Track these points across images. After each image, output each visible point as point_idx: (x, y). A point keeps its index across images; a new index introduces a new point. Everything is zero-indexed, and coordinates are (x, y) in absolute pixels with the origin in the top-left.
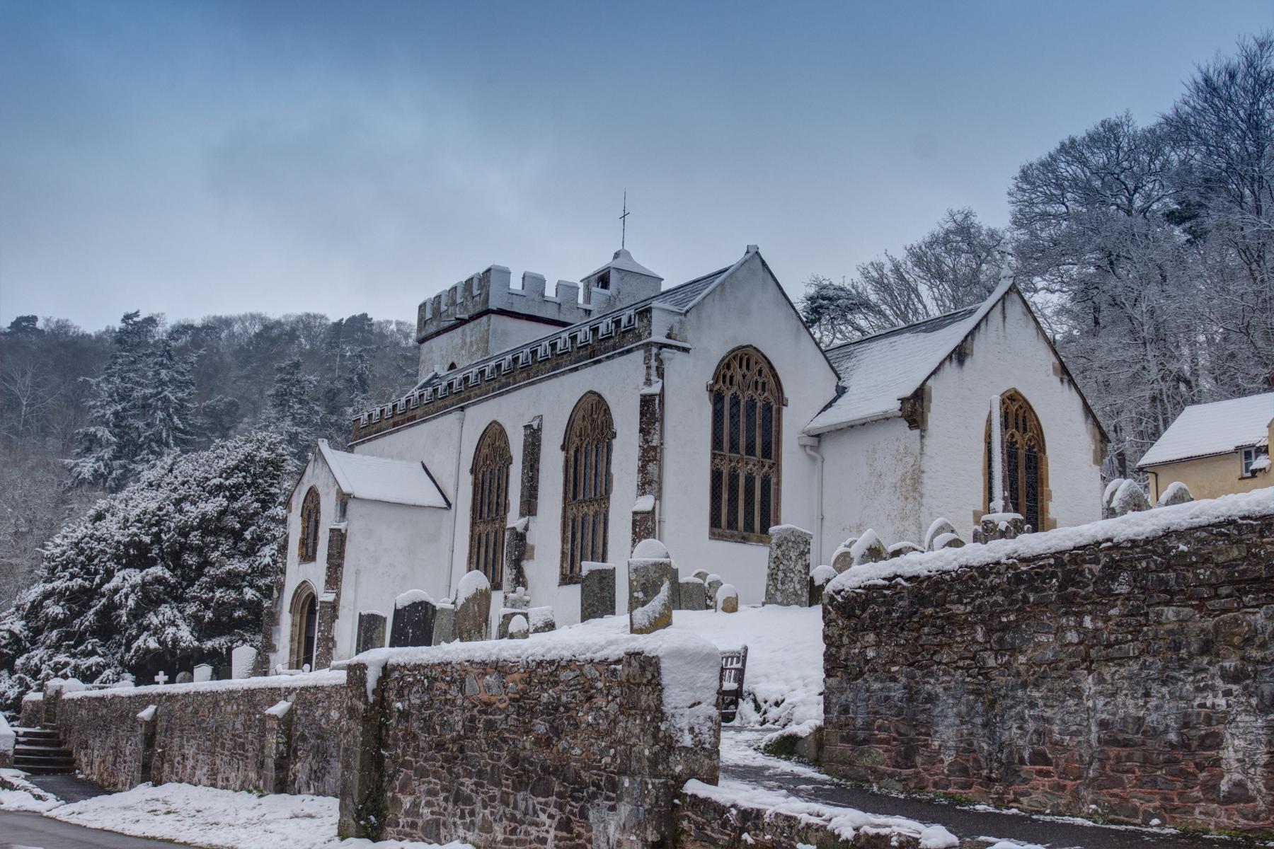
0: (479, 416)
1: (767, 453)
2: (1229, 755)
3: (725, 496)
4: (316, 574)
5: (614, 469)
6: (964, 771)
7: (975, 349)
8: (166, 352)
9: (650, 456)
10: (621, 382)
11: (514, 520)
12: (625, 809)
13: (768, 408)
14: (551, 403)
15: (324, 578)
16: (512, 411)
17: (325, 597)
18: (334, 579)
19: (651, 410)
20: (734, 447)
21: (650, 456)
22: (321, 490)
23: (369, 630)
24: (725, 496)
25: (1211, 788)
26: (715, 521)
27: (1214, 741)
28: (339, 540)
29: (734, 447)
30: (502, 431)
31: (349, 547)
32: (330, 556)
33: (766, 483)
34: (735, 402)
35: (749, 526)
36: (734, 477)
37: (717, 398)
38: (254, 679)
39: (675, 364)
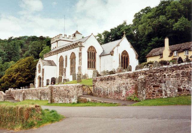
0: (60, 55)
1: (94, 59)
2: (123, 93)
3: (89, 64)
4: (41, 74)
5: (76, 62)
6: (104, 95)
7: (46, 81)
8: (14, 40)
9: (80, 60)
10: (76, 51)
11: (64, 67)
12: (74, 99)
13: (94, 53)
14: (68, 53)
15: (42, 75)
16: (63, 54)
17: (41, 77)
18: (43, 75)
19: (80, 54)
20: (90, 58)
21: (80, 60)
22: (41, 64)
23: (112, 53)
24: (89, 64)
25: (122, 96)
26: (88, 67)
27: (122, 92)
28: (43, 70)
29: (90, 58)
30: (62, 57)
31: (45, 71)
32: (42, 72)
33: (94, 63)
34: (90, 53)
35: (92, 68)
36: (90, 62)
37: (88, 52)
38: (77, 84)
39: (83, 49)
